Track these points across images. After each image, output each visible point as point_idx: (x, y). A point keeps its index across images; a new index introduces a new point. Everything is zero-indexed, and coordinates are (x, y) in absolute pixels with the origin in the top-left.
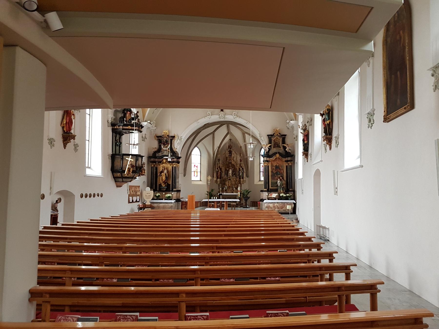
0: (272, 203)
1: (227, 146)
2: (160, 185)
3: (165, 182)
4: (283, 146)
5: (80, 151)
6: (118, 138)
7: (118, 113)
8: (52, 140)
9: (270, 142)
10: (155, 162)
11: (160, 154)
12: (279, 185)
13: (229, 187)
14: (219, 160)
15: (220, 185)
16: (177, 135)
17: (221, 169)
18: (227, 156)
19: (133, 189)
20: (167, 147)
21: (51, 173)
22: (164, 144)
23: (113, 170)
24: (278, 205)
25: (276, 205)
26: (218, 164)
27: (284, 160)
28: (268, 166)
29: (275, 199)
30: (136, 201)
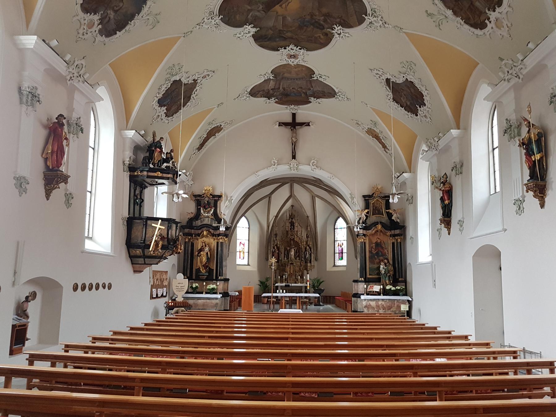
0: (374, 300)
1: (288, 216)
2: (198, 270)
3: (205, 266)
4: (388, 213)
5: (75, 206)
6: (137, 192)
7: (139, 152)
8: (22, 180)
9: (367, 206)
10: (191, 235)
11: (198, 223)
12: (383, 272)
13: (290, 275)
14: (276, 235)
15: (278, 272)
16: (225, 193)
17: (278, 248)
18: (288, 229)
19: (158, 276)
20: (208, 212)
21: (18, 243)
22: (205, 208)
23: (130, 244)
24: (383, 303)
25: (380, 303)
26: (274, 241)
27: (389, 233)
28: (365, 243)
29: (378, 294)
30: (162, 296)
